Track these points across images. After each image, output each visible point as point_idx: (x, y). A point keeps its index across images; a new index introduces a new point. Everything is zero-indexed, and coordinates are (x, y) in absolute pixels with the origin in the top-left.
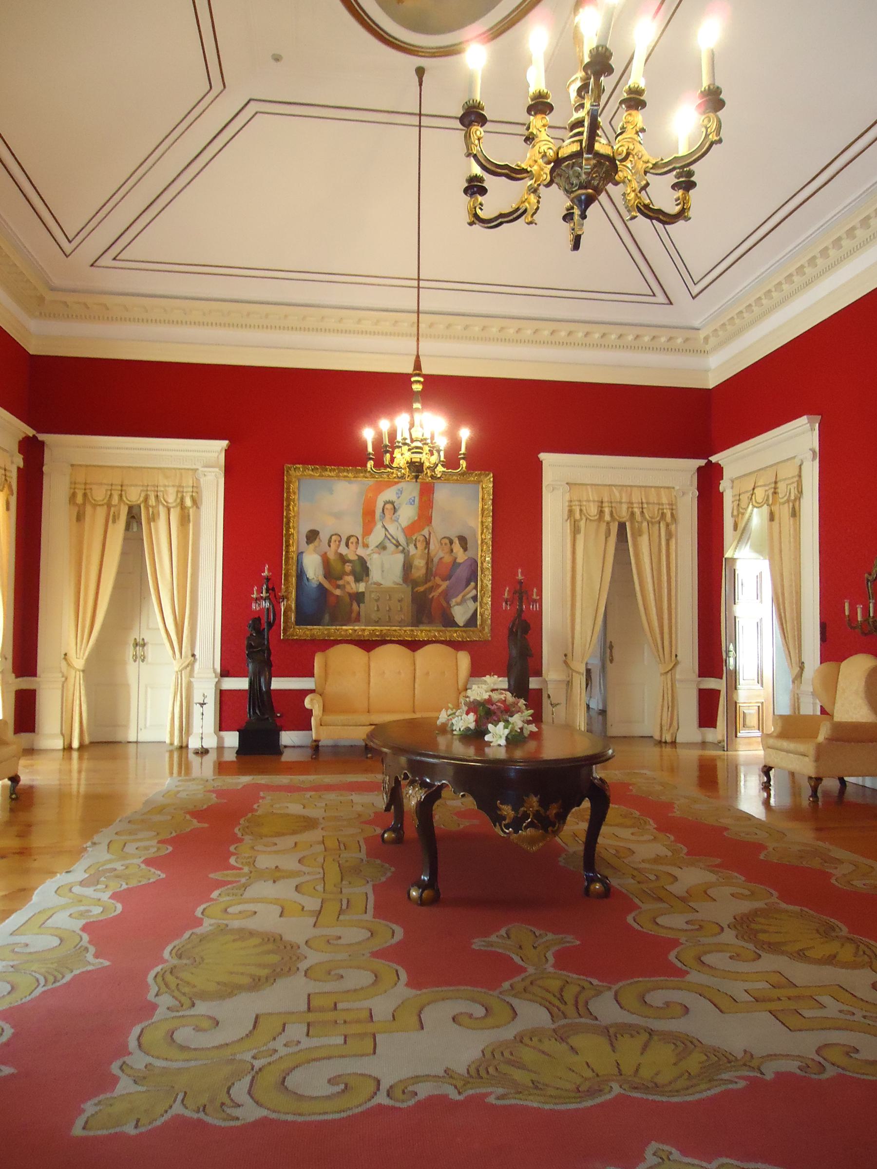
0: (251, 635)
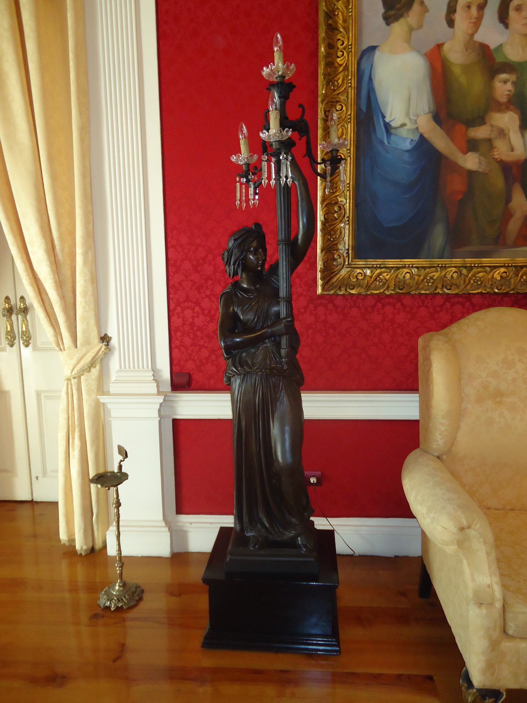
0: (236, 285)
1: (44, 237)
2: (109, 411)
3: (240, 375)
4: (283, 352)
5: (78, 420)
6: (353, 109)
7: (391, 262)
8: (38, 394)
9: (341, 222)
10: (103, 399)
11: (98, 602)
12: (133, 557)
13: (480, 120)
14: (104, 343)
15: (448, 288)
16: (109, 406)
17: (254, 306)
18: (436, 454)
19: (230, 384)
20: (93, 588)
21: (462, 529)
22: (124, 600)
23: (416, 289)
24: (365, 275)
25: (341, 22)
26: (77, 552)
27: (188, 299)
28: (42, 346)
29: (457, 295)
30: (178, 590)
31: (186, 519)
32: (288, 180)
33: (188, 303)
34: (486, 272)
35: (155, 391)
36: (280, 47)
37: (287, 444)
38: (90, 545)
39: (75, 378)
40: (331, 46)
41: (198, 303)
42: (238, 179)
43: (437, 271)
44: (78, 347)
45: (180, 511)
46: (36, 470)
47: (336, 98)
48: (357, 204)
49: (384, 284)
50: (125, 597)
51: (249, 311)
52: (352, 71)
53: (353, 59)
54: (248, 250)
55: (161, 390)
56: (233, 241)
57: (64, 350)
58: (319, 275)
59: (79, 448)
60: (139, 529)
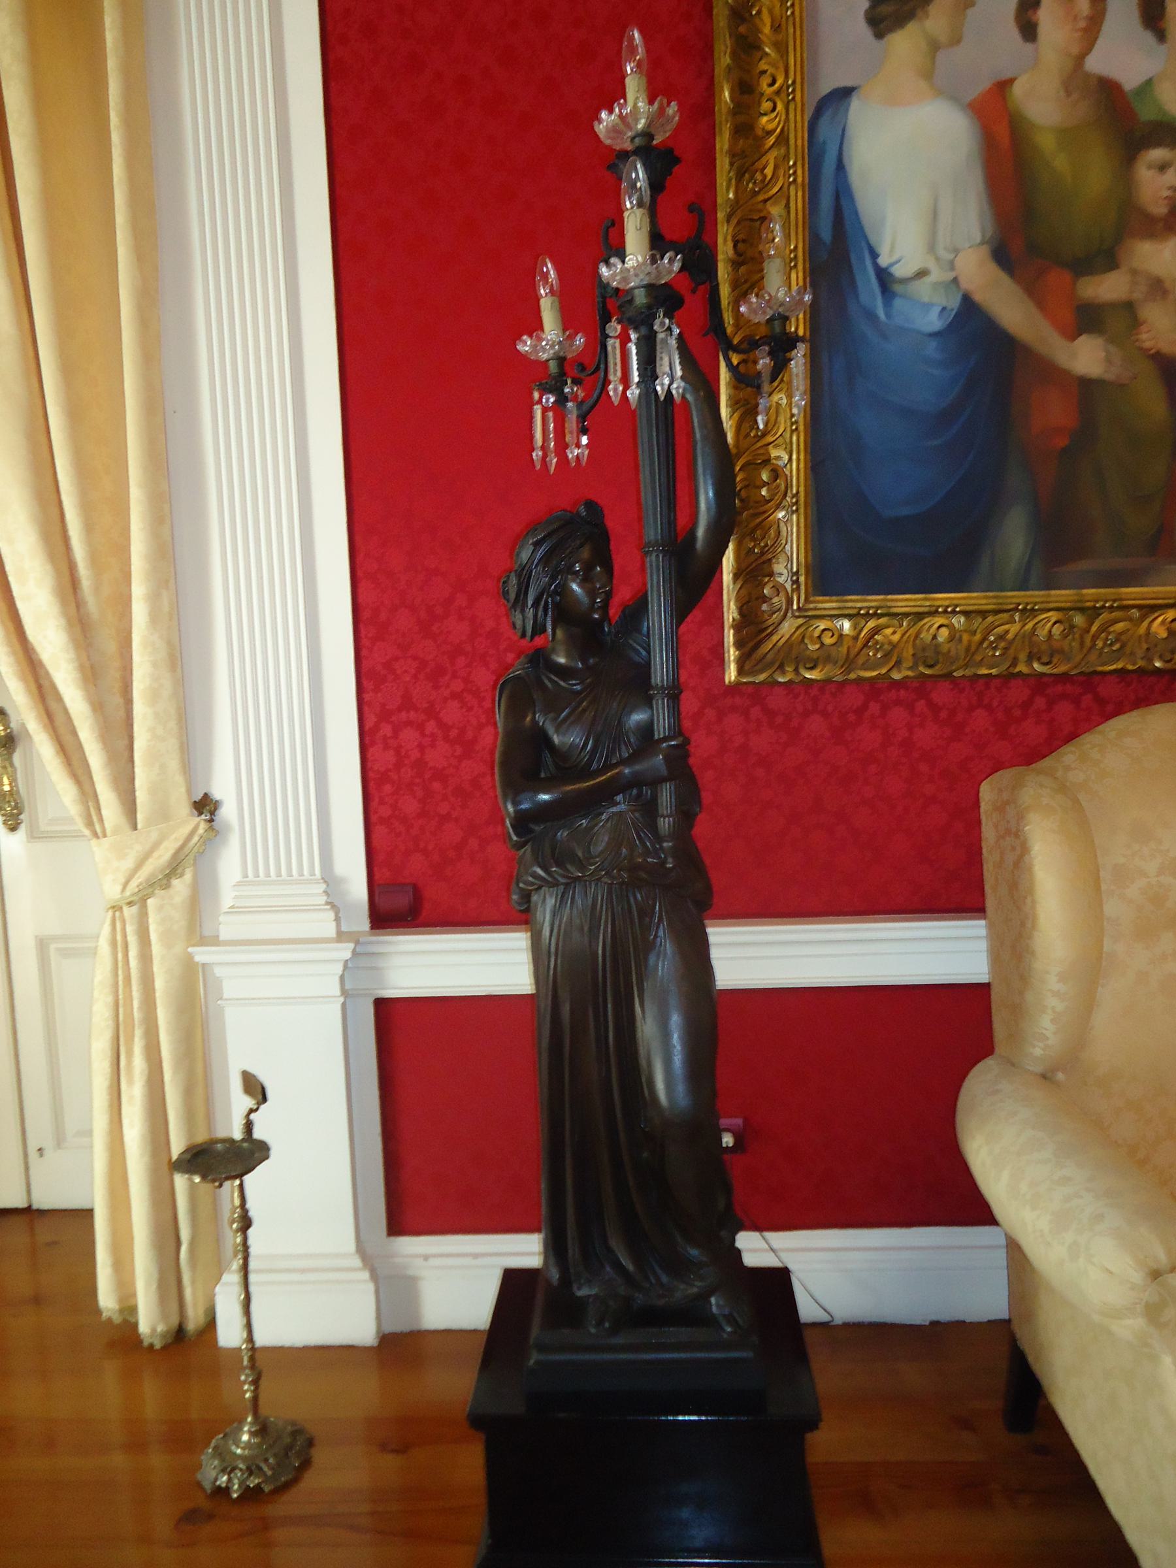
0: (540, 659)
1: (52, 556)
2: (219, 981)
3: (556, 884)
4: (665, 824)
5: (140, 1008)
6: (800, 237)
7: (904, 602)
8: (42, 945)
9: (778, 507)
10: (202, 955)
11: (199, 1476)
12: (281, 1348)
13: (1104, 257)
14: (203, 817)
15: (1045, 659)
16: (218, 972)
17: (584, 710)
18: (1039, 1069)
19: (527, 910)
20: (185, 1438)
21: (1155, 1275)
22: (266, 1469)
23: (966, 666)
24: (841, 636)
25: (767, 30)
26: (141, 1342)
27: (407, 703)
28: (49, 828)
29: (1064, 678)
30: (402, 1434)
31: (412, 1246)
32: (675, 386)
33: (408, 712)
34: (1131, 619)
35: (330, 930)
36: (639, 65)
37: (678, 1060)
38: (174, 1321)
39: (130, 904)
40: (746, 89)
41: (431, 712)
42: (536, 395)
43: (1012, 621)
44: (139, 826)
45: (397, 1225)
46: (40, 1131)
47: (760, 211)
48: (817, 465)
49: (887, 655)
50: (266, 1460)
51: (572, 723)
52: (796, 146)
53: (799, 118)
54: (569, 569)
55: (344, 929)
56: (532, 548)
57: (105, 836)
58: (730, 636)
59: (145, 1078)
60: (295, 1277)
